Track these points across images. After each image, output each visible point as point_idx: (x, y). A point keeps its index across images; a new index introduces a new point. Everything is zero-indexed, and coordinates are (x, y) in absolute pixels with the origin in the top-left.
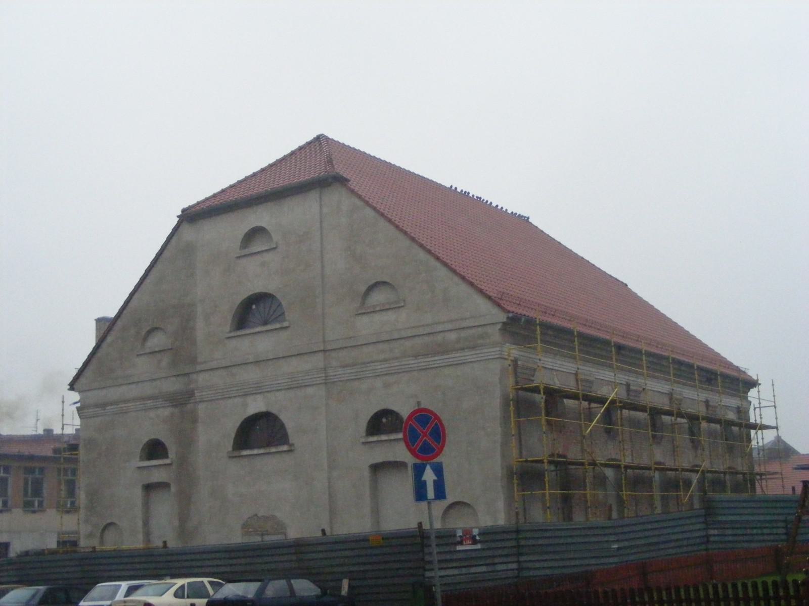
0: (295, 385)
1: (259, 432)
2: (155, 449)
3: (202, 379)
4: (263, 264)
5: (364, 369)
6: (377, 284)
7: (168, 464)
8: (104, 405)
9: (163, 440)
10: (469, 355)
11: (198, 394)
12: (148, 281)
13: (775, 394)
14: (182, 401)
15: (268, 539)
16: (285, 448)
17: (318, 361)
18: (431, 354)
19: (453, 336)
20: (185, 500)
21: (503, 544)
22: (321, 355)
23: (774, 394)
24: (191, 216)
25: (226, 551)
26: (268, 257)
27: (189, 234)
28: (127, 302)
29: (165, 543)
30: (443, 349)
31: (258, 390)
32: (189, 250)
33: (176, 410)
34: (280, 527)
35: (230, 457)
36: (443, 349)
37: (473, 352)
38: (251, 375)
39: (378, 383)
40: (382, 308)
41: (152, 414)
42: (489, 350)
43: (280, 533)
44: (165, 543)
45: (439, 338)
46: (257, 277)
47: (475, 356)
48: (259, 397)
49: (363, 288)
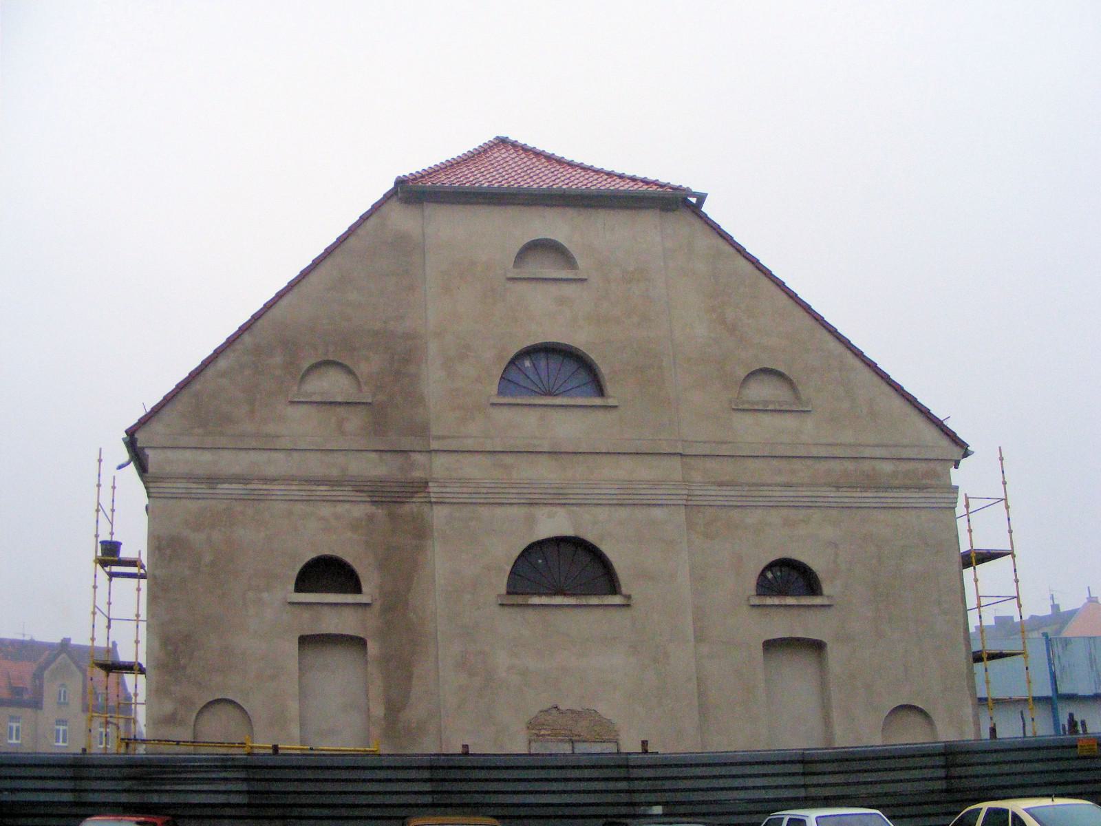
0: (629, 499)
1: (568, 569)
2: (327, 574)
3: (440, 465)
4: (561, 301)
5: (756, 493)
6: (766, 371)
7: (366, 605)
8: (212, 480)
9: (349, 559)
10: (914, 497)
11: (436, 490)
12: (313, 277)
13: (97, 584)
14: (397, 497)
15: (581, 748)
16: (617, 600)
17: (673, 468)
18: (860, 487)
19: (887, 467)
20: (399, 671)
21: (32, 771)
22: (676, 462)
23: (95, 582)
24: (411, 192)
25: (71, 766)
26: (569, 290)
27: (403, 219)
28: (269, 306)
29: (644, 743)
30: (872, 483)
31: (558, 499)
32: (406, 249)
33: (380, 512)
34: (606, 731)
35: (502, 605)
36: (872, 483)
37: (921, 495)
38: (545, 472)
39: (775, 517)
40: (778, 408)
41: (326, 510)
42: (944, 495)
43: (609, 741)
44: (644, 743)
45: (866, 466)
46: (548, 315)
47: (923, 500)
48: (561, 512)
49: (742, 373)
